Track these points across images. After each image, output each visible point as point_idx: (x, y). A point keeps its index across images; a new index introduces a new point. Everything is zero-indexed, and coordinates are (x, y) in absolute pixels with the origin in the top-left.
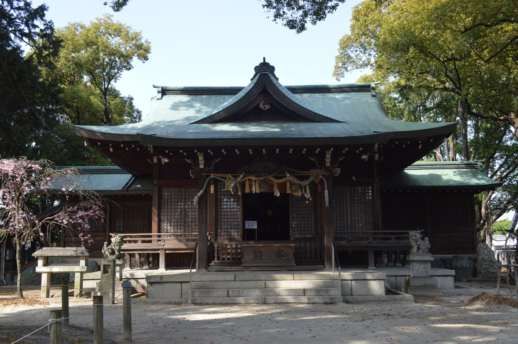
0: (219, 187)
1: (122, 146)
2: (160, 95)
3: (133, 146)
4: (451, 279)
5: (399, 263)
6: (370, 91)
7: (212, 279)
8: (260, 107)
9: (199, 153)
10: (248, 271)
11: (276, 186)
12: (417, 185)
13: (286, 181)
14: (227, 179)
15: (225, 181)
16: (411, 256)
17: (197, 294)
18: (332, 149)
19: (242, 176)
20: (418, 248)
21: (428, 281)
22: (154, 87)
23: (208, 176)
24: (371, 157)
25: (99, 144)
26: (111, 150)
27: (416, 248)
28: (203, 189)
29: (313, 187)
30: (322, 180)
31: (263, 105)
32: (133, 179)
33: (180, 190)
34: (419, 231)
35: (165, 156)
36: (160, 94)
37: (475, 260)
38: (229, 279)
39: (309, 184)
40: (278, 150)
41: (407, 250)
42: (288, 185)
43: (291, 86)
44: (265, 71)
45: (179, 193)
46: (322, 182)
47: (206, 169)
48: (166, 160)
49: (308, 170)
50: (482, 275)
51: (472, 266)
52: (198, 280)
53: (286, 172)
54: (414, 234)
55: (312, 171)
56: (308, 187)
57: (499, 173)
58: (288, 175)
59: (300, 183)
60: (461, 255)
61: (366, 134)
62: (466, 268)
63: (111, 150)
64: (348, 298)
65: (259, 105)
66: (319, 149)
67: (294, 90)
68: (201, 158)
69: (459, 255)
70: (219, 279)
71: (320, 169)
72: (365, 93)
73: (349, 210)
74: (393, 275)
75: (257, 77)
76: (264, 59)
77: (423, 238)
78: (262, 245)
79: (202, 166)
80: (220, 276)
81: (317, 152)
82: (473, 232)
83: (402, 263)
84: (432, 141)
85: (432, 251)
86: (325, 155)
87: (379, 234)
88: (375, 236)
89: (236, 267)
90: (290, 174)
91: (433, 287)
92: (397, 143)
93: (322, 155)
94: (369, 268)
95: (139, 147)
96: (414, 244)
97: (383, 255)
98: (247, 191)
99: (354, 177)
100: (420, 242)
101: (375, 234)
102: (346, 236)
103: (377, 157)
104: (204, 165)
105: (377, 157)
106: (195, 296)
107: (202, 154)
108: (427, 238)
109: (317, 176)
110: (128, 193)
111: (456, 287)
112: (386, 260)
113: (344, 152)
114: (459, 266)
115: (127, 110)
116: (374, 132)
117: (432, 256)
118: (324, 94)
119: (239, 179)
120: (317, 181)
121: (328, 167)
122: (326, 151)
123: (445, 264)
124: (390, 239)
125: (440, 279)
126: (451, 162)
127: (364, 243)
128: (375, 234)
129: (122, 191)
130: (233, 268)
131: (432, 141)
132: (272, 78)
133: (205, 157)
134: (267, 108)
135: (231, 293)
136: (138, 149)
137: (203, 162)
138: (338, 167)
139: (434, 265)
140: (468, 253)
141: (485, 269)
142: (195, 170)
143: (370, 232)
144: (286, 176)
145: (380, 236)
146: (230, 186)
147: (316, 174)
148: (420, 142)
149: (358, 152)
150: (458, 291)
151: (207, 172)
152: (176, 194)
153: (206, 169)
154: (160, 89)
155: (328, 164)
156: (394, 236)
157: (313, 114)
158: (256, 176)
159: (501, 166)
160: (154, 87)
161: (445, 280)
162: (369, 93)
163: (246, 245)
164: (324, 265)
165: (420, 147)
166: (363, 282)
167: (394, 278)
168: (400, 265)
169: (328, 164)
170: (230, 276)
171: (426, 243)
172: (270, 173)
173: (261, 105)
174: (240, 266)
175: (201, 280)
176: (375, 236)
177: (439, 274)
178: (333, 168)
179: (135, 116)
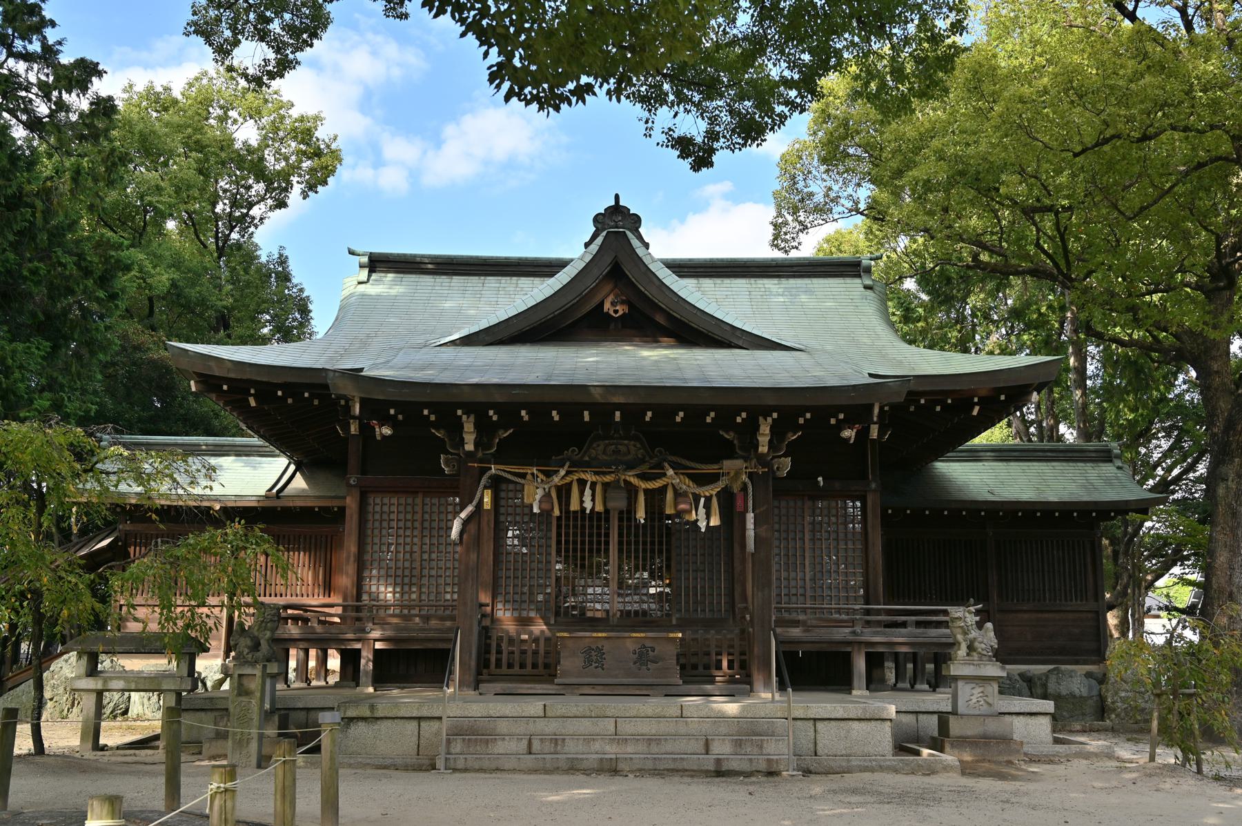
0: (503, 494)
1: (280, 393)
2: (365, 272)
3: (306, 395)
4: (1046, 722)
5: (922, 683)
6: (859, 276)
7: (492, 713)
8: (605, 310)
9: (464, 417)
10: (573, 694)
11: (641, 498)
12: (966, 498)
13: (665, 487)
14: (529, 477)
15: (522, 481)
16: (952, 667)
17: (457, 747)
18: (775, 415)
19: (562, 472)
20: (971, 648)
21: (993, 726)
22: (351, 253)
23: (483, 471)
24: (863, 434)
25: (225, 387)
26: (253, 403)
27: (964, 646)
28: (474, 503)
29: (727, 499)
30: (745, 484)
31: (613, 304)
32: (292, 467)
33: (410, 501)
34: (972, 609)
35: (385, 420)
36: (366, 271)
37: (1102, 680)
38: (532, 713)
39: (718, 494)
40: (649, 414)
41: (942, 655)
42: (670, 495)
43: (674, 260)
44: (617, 224)
45: (409, 508)
46: (744, 488)
47: (480, 454)
48: (387, 431)
49: (717, 460)
50: (1117, 716)
51: (1095, 693)
52: (459, 713)
53: (666, 465)
54: (958, 615)
55: (728, 465)
56: (715, 500)
57: (1160, 471)
58: (671, 472)
59: (698, 491)
60: (1069, 667)
61: (854, 383)
62: (1081, 697)
63: (253, 403)
64: (809, 761)
65: (602, 304)
66: (744, 415)
67: (684, 269)
68: (469, 426)
69: (1063, 667)
70: (508, 713)
71: (746, 459)
72: (848, 280)
73: (807, 555)
74: (910, 709)
75: (599, 240)
76: (617, 197)
77: (980, 625)
78: (604, 635)
79: (469, 447)
80: (510, 706)
81: (739, 420)
82: (1097, 612)
83: (929, 683)
84: (1003, 397)
85: (1002, 655)
86: (757, 428)
87: (878, 612)
88: (869, 618)
89: (545, 686)
90: (674, 469)
91: (1005, 740)
92: (923, 401)
93: (751, 428)
94: (854, 692)
95: (318, 396)
96: (960, 637)
97: (886, 664)
98: (574, 506)
99: (820, 479)
100: (974, 634)
101: (868, 612)
102: (801, 617)
103: (874, 432)
104: (476, 445)
105: (874, 432)
106: (453, 751)
107: (472, 418)
108: (989, 625)
109: (738, 474)
110: (279, 504)
111: (1057, 741)
112: (891, 676)
113: (801, 421)
114: (1064, 692)
115: (270, 299)
116: (871, 375)
117: (1003, 669)
118: (752, 281)
119: (556, 480)
120: (736, 488)
121: (762, 454)
122: (761, 419)
123: (1033, 687)
124: (904, 625)
125: (1018, 722)
126: (1046, 444)
127: (843, 633)
128: (868, 612)
129: (266, 497)
130: (539, 688)
131: (1003, 397)
132: (635, 242)
133: (477, 426)
134: (620, 313)
135: (536, 745)
136: (316, 402)
137: (473, 437)
138: (785, 455)
139: (1007, 688)
140: (1085, 663)
141: (1123, 700)
142: (452, 454)
143: (857, 607)
144: (665, 475)
145: (879, 618)
146: (535, 496)
147: (735, 469)
148: (976, 400)
149: (833, 421)
150: (1060, 748)
151: (481, 461)
152: (401, 508)
153: (480, 454)
154: (365, 259)
155: (763, 449)
156: (914, 618)
157: (728, 328)
158: (596, 473)
159: (1166, 455)
160: (351, 253)
161: (1032, 725)
162: (858, 281)
163: (566, 635)
164: (750, 683)
165: (975, 412)
166: (842, 724)
167: (911, 718)
168: (926, 687)
169: (763, 449)
170: (534, 707)
171: (988, 637)
172: (630, 466)
173: (607, 306)
174: (552, 682)
175: (466, 714)
176: (869, 618)
177: (1017, 710)
178: (774, 457)
179: (291, 318)
